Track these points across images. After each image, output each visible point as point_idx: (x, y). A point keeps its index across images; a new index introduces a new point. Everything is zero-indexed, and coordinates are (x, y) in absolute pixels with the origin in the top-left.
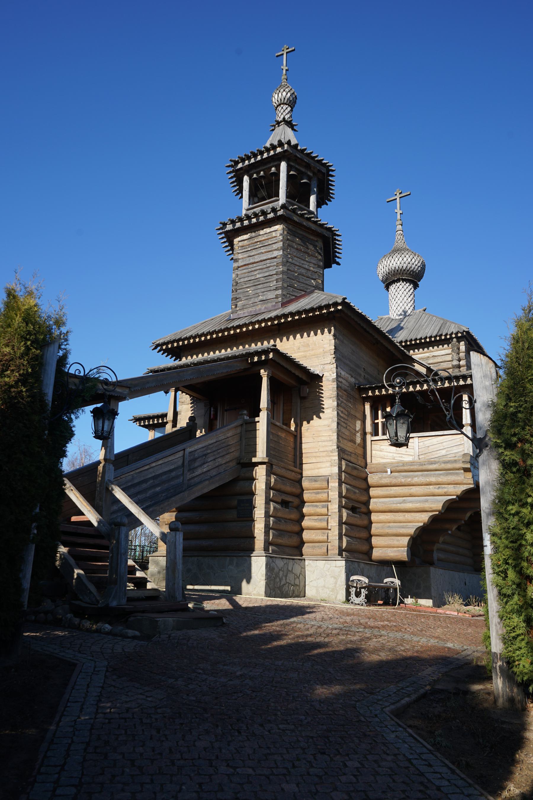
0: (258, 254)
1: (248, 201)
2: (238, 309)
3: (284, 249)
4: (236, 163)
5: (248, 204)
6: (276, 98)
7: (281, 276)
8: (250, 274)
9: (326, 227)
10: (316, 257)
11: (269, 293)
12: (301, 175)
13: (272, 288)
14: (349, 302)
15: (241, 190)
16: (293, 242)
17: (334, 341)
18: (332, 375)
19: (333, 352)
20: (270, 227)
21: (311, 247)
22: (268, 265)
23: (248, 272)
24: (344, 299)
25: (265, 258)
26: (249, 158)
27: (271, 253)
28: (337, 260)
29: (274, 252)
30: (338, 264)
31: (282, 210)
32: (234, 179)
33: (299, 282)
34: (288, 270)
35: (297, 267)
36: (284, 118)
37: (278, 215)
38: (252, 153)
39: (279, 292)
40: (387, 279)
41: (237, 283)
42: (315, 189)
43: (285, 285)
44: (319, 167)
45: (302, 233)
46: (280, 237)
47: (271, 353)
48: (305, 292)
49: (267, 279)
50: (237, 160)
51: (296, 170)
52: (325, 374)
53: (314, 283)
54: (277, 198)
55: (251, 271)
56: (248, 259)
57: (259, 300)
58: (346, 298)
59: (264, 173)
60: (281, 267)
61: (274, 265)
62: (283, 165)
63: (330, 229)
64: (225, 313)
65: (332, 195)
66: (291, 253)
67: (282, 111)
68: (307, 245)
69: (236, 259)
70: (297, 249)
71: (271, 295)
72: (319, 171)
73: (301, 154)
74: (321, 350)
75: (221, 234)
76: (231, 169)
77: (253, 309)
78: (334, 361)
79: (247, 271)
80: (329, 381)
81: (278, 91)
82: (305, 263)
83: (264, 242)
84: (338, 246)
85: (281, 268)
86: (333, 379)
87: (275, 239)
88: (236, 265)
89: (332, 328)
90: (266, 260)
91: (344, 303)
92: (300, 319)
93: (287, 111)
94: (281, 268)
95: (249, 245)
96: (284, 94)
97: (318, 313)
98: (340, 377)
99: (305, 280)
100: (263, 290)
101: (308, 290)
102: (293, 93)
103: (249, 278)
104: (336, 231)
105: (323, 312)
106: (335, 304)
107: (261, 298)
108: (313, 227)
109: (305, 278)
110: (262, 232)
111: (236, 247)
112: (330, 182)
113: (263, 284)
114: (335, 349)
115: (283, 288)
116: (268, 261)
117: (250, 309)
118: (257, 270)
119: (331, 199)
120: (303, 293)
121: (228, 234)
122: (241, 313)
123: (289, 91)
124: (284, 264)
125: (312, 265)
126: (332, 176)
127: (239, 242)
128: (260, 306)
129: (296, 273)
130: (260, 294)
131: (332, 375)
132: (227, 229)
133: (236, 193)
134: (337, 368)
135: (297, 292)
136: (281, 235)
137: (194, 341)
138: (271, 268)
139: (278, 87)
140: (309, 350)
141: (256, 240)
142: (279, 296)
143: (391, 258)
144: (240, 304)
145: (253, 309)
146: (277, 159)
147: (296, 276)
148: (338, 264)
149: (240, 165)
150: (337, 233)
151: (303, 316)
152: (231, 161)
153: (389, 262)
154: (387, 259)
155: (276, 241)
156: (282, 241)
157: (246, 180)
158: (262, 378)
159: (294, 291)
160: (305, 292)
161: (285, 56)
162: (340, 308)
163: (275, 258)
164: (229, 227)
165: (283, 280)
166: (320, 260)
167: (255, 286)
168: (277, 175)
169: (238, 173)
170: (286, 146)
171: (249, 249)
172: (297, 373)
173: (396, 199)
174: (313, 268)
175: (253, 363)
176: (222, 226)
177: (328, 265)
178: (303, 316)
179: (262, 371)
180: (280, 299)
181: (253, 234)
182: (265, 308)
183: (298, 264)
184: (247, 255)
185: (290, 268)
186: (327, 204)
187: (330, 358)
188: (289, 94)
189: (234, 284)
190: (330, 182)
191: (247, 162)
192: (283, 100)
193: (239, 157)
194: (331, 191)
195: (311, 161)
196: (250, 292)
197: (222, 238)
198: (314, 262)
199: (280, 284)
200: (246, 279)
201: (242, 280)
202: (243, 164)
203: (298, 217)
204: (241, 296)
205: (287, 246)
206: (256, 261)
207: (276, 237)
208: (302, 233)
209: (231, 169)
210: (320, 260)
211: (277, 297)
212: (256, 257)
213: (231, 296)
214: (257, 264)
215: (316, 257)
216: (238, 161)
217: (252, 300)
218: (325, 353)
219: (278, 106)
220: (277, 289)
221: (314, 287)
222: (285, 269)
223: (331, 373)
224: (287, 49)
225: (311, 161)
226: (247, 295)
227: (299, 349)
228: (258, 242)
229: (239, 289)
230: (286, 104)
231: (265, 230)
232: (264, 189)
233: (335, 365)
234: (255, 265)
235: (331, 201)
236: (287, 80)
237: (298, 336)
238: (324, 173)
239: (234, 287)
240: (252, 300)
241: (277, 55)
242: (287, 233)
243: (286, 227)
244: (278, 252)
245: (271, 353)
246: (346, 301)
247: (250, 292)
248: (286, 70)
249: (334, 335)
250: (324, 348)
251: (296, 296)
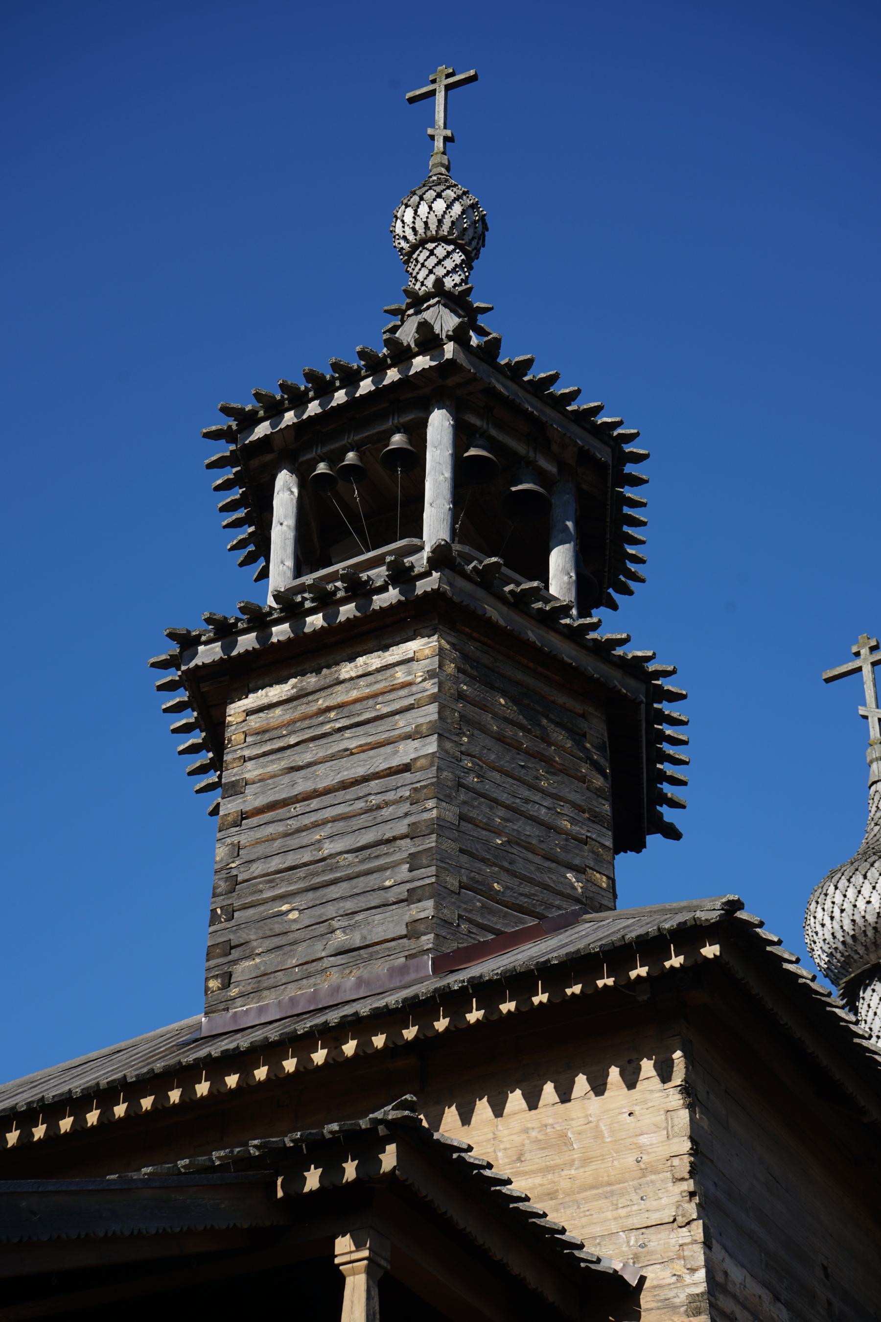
0: (332, 757)
1: (290, 563)
2: (234, 992)
3: (442, 730)
4: (249, 421)
5: (290, 574)
6: (408, 221)
7: (431, 842)
8: (293, 842)
9: (622, 658)
10: (582, 779)
11: (378, 917)
12: (515, 466)
13: (391, 896)
14: (755, 920)
15: (261, 545)
16: (484, 708)
17: (685, 1114)
18: (688, 1279)
19: (683, 1165)
20: (385, 648)
21: (559, 736)
22: (375, 800)
23: (286, 835)
24: (734, 906)
25: (361, 771)
26: (299, 401)
27: (388, 749)
28: (668, 814)
29: (402, 746)
30: (672, 833)
31: (436, 575)
32: (237, 493)
33: (513, 874)
34: (462, 817)
35: (501, 812)
36: (439, 282)
37: (419, 591)
38: (310, 376)
39: (426, 909)
40: (847, 962)
41: (234, 882)
42: (570, 524)
43: (452, 882)
44: (582, 438)
45: (519, 676)
46: (428, 685)
47: (391, 1148)
48: (541, 917)
49: (369, 858)
50: (248, 408)
51: (491, 444)
52: (653, 1276)
53: (578, 885)
54: (416, 541)
55: (299, 831)
56: (286, 779)
57: (330, 950)
58: (737, 905)
59: (361, 455)
60: (430, 804)
61: (402, 799)
62: (439, 424)
63: (636, 667)
64: (175, 1026)
65: (632, 567)
66: (476, 750)
67: (432, 261)
68: (544, 728)
69: (233, 784)
70: (500, 739)
71: (388, 925)
72: (585, 456)
73: (509, 383)
74: (630, 1160)
75: (170, 687)
76: (226, 449)
77: (306, 989)
78: (691, 1209)
79: (280, 828)
80: (674, 1308)
81: (416, 198)
82: (537, 797)
83: (358, 706)
84: (670, 750)
85: (431, 810)
86: (693, 1298)
87: (402, 693)
88: (230, 807)
89: (678, 1054)
90: (366, 779)
91: (732, 927)
92: (527, 1015)
93: (449, 264)
94: (431, 810)
95: (293, 722)
96: (440, 206)
97: (610, 982)
98: (724, 1290)
99: (539, 868)
100: (350, 905)
101: (554, 913)
102: (473, 206)
103: (291, 860)
104: (666, 674)
105: (633, 974)
106: (689, 935)
107: (340, 938)
108: (568, 652)
109: (538, 860)
110: (347, 670)
111: (234, 735)
112: (627, 510)
113: (349, 878)
114: (695, 1151)
115: (438, 892)
116: (373, 783)
117: (291, 991)
118: (325, 822)
119: (632, 584)
120: (532, 922)
121: (205, 688)
122: (247, 1011)
123: (458, 198)
124: (443, 792)
125: (567, 810)
126: (637, 482)
127: (249, 713)
128: (334, 977)
129: (499, 834)
130: (335, 924)
131: (688, 1279)
132: (198, 661)
133: (242, 554)
134: (707, 1244)
135: (505, 916)
136: (431, 674)
137: (26, 1135)
138: (386, 812)
139: (417, 186)
140: (572, 1163)
141: (322, 703)
142: (422, 927)
143: (858, 879)
144: (243, 970)
145: (306, 989)
146: (410, 402)
147: (497, 847)
148: (672, 833)
149: (263, 430)
150: (669, 684)
151: (536, 1000)
152: (227, 411)
153: (851, 893)
154: (843, 883)
155: (411, 700)
156: (434, 698)
157: (285, 492)
158: (340, 1280)
159: (492, 912)
160: (541, 917)
161: (440, 97)
162: (710, 951)
163: (406, 768)
164: (208, 653)
165: (441, 859)
166: (598, 793)
167: (314, 888)
168: (414, 460)
169: (255, 463)
170: (449, 349)
171: (292, 740)
172: (517, 1264)
173: (859, 669)
174: (573, 821)
175: (298, 1199)
176: (175, 648)
177: (630, 839)
178: (536, 1000)
179: (343, 1244)
180: (427, 940)
181: (311, 681)
182: (360, 982)
183: (504, 797)
184: (284, 764)
185: (473, 814)
186: (614, 606)
187: (672, 1196)
188: (457, 209)
189: (223, 886)
190: (627, 510)
191: (289, 417)
192: (433, 226)
193: (258, 396)
194: (631, 550)
195: (550, 415)
196: (294, 915)
197: (178, 708)
198: (572, 796)
199: (427, 875)
200: (275, 864)
201: (257, 868)
202: (273, 426)
203: (504, 609)
204: (251, 935)
205: (456, 721)
206: (321, 785)
207: (410, 684)
208: (519, 676)
209: (226, 449)
210: (598, 793)
211: (413, 931)
212: (321, 769)
213: (206, 936)
214: (328, 799)
215: (582, 779)
216: (254, 412)
217: (302, 952)
218: (644, 1172)
219: (414, 248)
220: (413, 897)
221: (577, 900)
222: (451, 813)
223: (678, 1267)
224: (448, 76)
225: (550, 415)
226: (278, 928)
227: (519, 1160)
228: (329, 709)
229: (245, 907)
230: (448, 242)
231: (361, 660)
232: (358, 507)
233: (698, 1230)
234: (315, 803)
235: (630, 593)
236: (448, 169)
237: (516, 1099)
238: (604, 465)
239: (221, 901)
240: (302, 952)
241: (409, 95)
242: (459, 670)
243: (452, 645)
244: (416, 744)
245: (391, 1148)
246: (741, 915)
247: (294, 915)
248: (446, 139)
249: (687, 1090)
250: (640, 1148)
251: (498, 933)
